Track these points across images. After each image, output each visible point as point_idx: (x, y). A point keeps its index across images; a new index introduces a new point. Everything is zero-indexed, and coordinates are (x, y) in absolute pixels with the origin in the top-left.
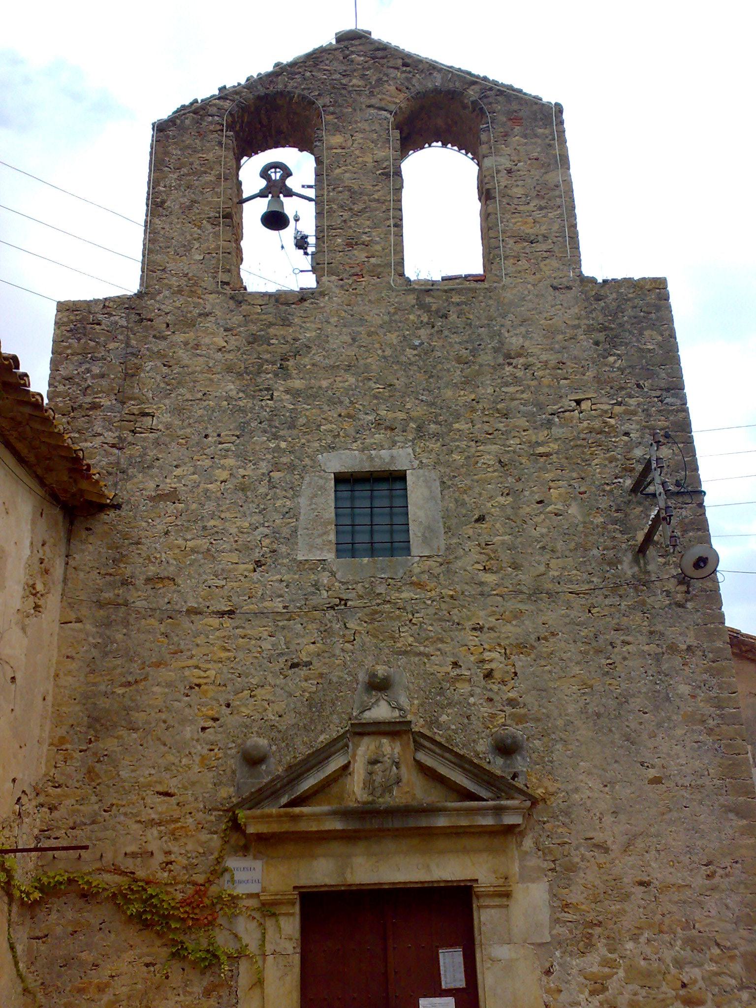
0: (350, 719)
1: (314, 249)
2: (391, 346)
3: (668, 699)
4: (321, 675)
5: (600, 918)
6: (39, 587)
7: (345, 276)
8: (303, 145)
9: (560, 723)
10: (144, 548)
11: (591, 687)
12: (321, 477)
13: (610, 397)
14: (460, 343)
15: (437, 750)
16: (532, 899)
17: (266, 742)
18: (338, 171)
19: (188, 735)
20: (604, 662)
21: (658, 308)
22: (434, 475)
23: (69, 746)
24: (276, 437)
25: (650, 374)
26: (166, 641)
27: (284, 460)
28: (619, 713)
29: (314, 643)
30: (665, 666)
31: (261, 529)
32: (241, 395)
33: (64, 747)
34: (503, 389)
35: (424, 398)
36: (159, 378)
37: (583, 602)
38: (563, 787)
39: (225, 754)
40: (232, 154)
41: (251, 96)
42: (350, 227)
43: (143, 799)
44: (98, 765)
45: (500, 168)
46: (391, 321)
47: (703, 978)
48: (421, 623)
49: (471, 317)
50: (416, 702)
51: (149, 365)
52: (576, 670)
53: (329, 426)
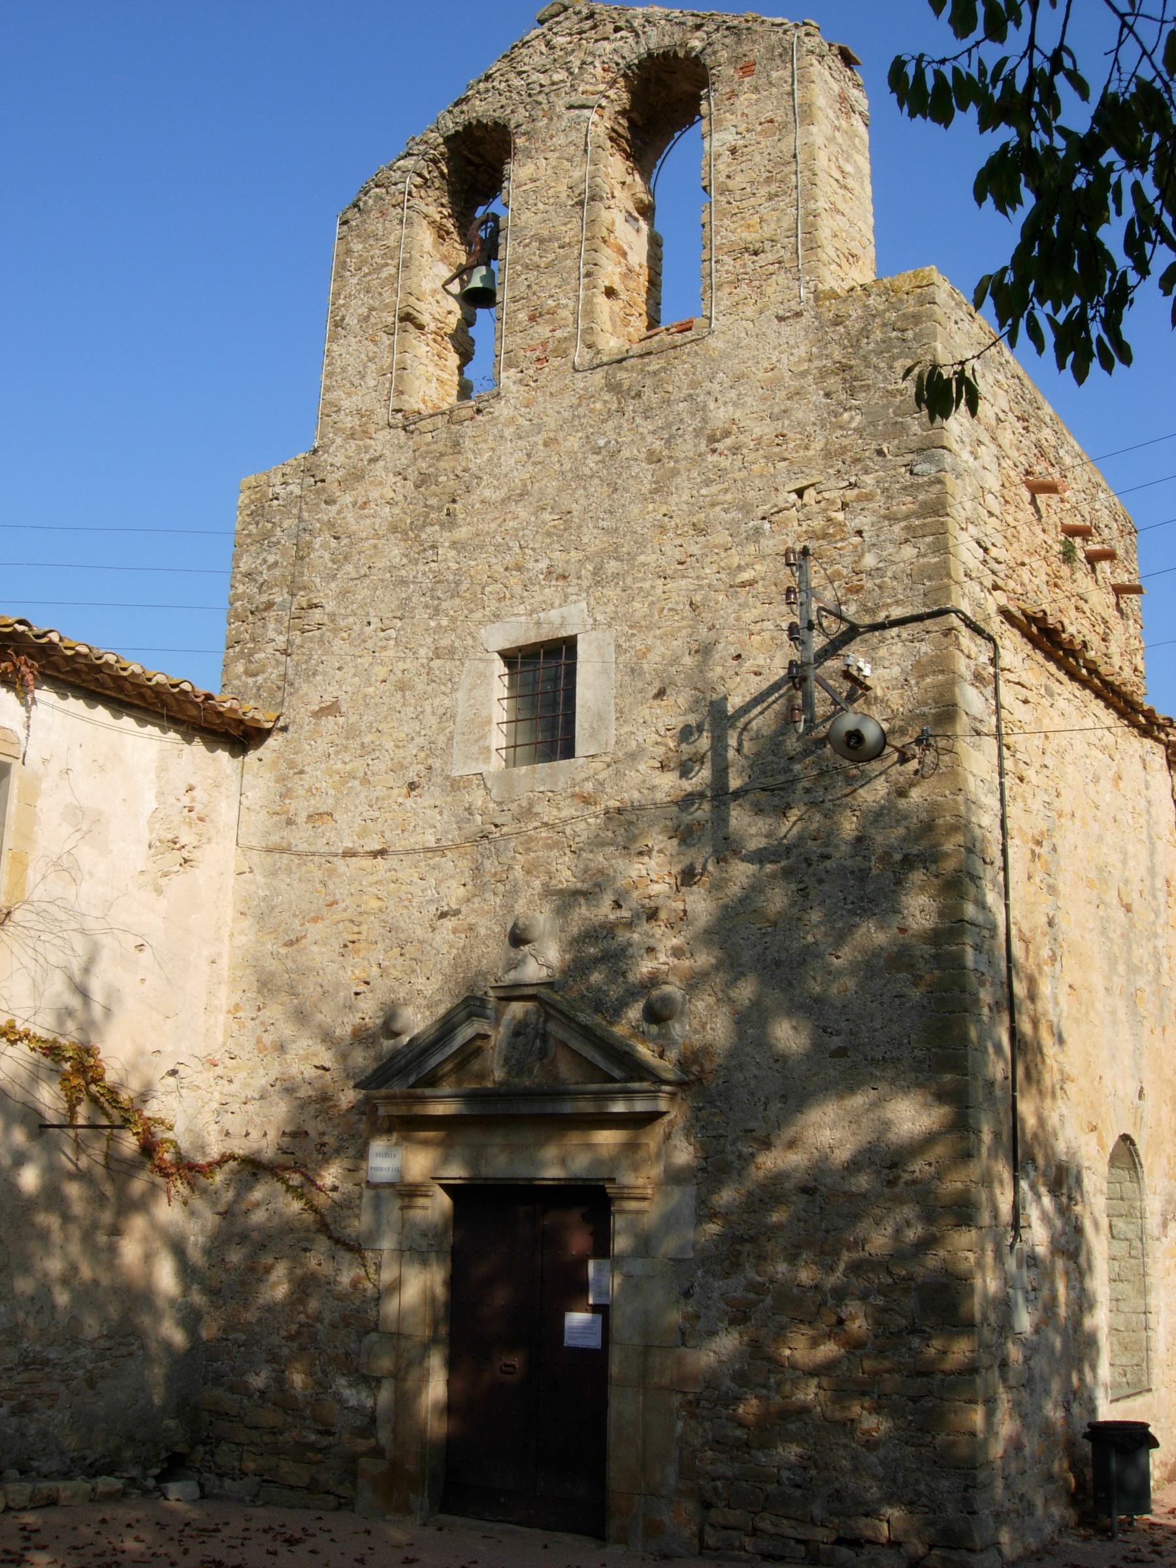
5: (752, 1233)
35: (605, 524)
49: (670, 389)
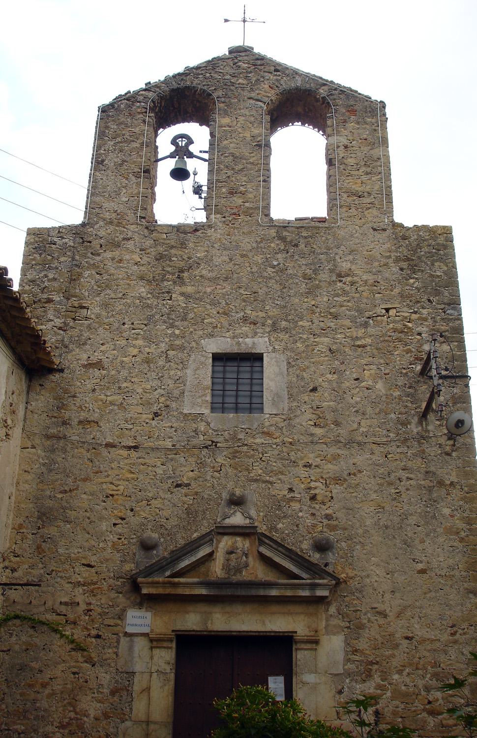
0: (215, 523)
1: (206, 195)
2: (257, 264)
3: (434, 517)
4: (196, 494)
5: (377, 659)
6: (9, 422)
7: (227, 215)
8: (204, 120)
9: (360, 531)
10: (78, 400)
11: (383, 508)
12: (203, 356)
13: (408, 306)
14: (306, 265)
15: (274, 546)
16: (333, 646)
17: (157, 535)
18: (226, 142)
19: (104, 528)
20: (393, 491)
21: (445, 247)
22: (283, 357)
23: (25, 530)
24: (172, 326)
25: (437, 293)
26: (91, 464)
27: (178, 342)
28: (401, 526)
29: (192, 471)
30: (435, 495)
31: (159, 390)
32: (149, 296)
33: (22, 531)
34: (335, 299)
35: (279, 303)
36: (93, 282)
37: (382, 450)
38: (359, 573)
39: (129, 542)
40: (152, 129)
41: (167, 89)
42: (232, 181)
43: (73, 568)
44: (44, 544)
45: (340, 144)
46: (258, 247)
47: (443, 698)
48: (268, 461)
49: (315, 246)
50: (261, 514)
51: (87, 273)
52: (374, 496)
53: (209, 320)
